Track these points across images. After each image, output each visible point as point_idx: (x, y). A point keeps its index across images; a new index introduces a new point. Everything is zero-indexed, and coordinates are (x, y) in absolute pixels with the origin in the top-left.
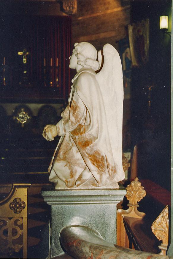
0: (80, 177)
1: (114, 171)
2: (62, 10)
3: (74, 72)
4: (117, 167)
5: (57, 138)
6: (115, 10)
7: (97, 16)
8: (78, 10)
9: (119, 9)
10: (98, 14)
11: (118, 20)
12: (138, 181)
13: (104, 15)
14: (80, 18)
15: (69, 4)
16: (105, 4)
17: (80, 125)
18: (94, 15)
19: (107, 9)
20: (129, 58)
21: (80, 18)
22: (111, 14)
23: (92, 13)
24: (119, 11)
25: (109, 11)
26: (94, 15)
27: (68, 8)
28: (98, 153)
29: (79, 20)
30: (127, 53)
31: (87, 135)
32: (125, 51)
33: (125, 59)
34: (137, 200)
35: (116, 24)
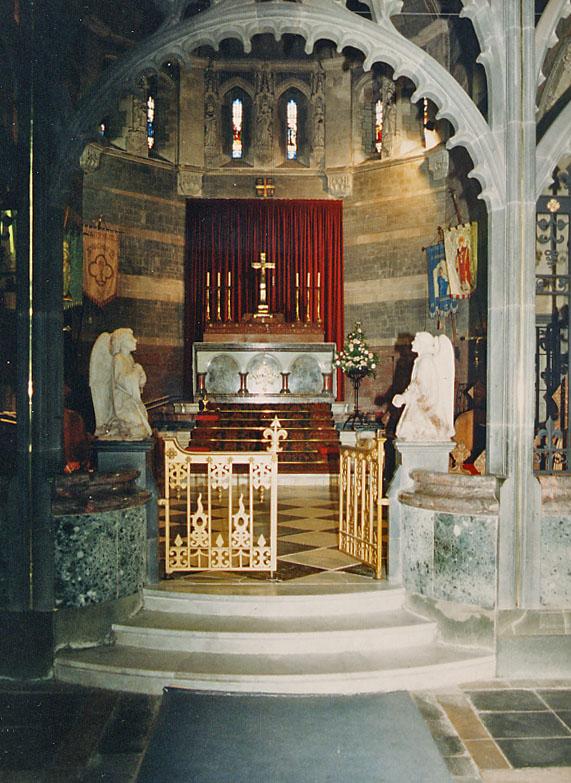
0: (423, 433)
1: (448, 429)
2: (326, 189)
3: (416, 355)
4: (212, 691)
5: (404, 406)
6: (420, 192)
7: (389, 201)
8: (354, 190)
9: (428, 191)
10: (390, 198)
11: (425, 209)
12: (562, 19)
13: (400, 201)
14: (358, 204)
15: (339, 181)
16: (402, 182)
17: (423, 396)
18: (383, 200)
19: (406, 190)
20: (444, 277)
21: (358, 204)
22: (412, 198)
23: (379, 195)
24: (427, 195)
25: (409, 195)
26: (383, 200)
27: (337, 187)
28: (435, 416)
29: (357, 207)
30: (441, 268)
31: (428, 404)
32: (438, 266)
33: (438, 280)
34: (463, 459)
35: (422, 217)
